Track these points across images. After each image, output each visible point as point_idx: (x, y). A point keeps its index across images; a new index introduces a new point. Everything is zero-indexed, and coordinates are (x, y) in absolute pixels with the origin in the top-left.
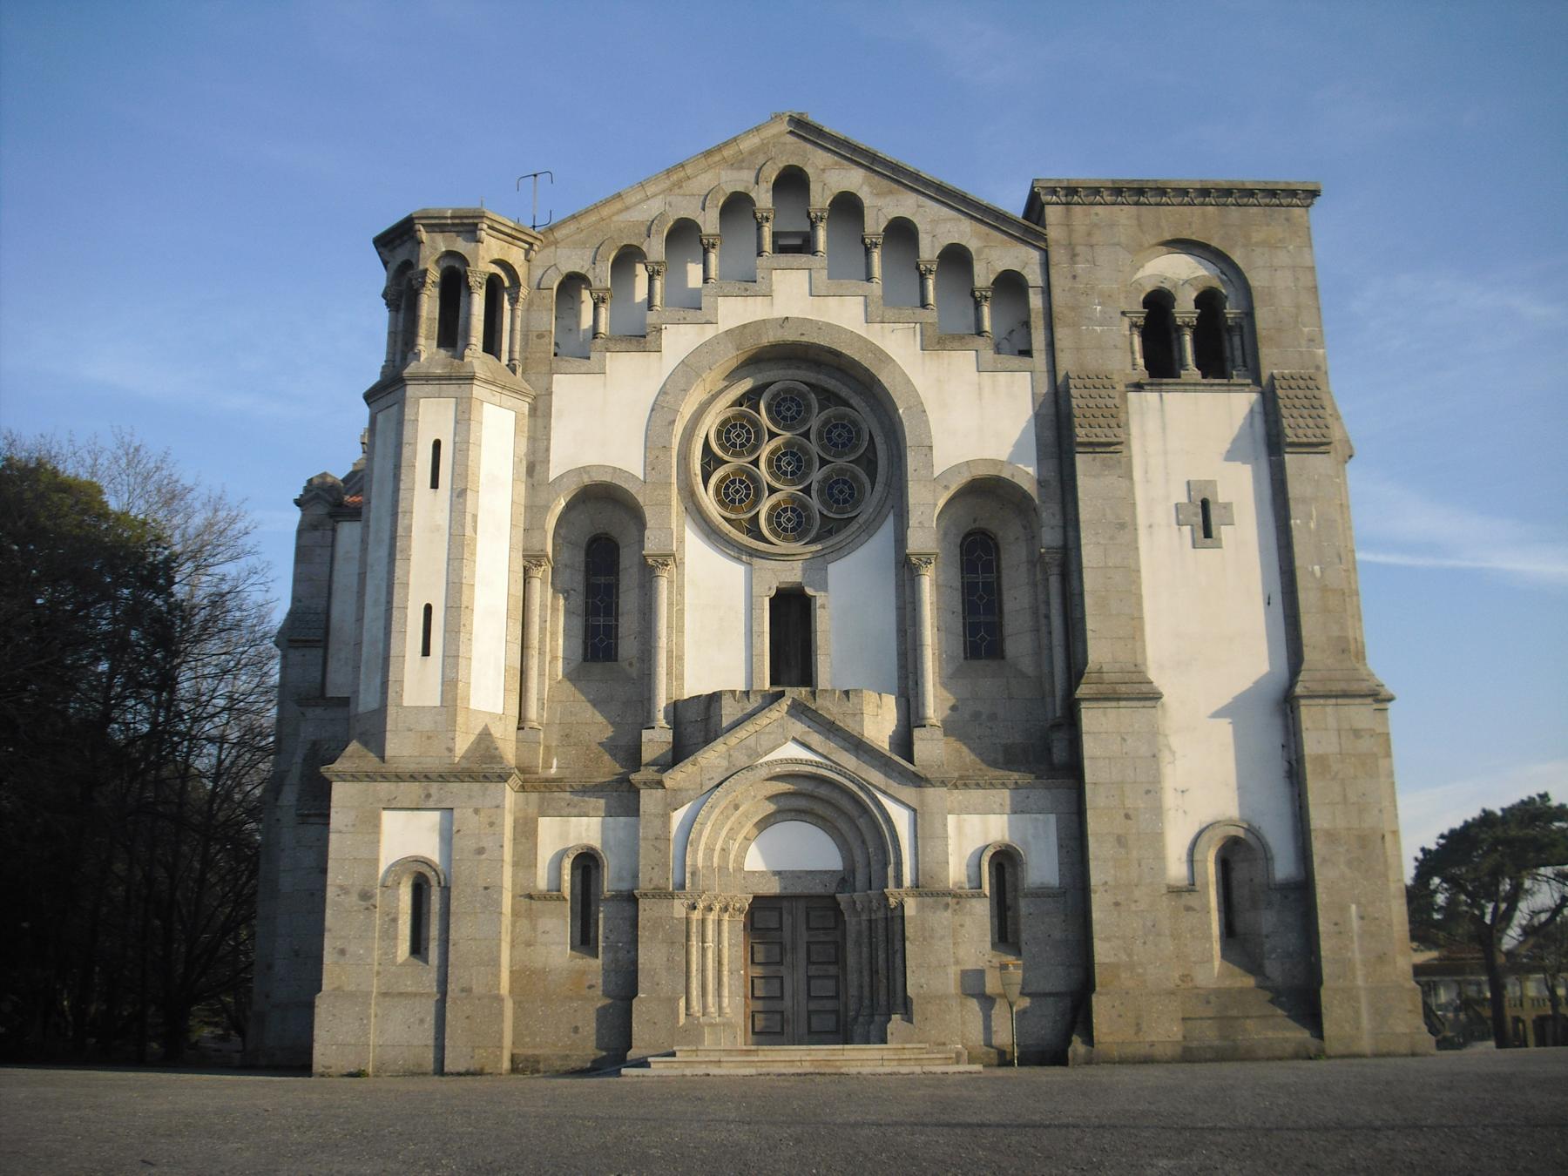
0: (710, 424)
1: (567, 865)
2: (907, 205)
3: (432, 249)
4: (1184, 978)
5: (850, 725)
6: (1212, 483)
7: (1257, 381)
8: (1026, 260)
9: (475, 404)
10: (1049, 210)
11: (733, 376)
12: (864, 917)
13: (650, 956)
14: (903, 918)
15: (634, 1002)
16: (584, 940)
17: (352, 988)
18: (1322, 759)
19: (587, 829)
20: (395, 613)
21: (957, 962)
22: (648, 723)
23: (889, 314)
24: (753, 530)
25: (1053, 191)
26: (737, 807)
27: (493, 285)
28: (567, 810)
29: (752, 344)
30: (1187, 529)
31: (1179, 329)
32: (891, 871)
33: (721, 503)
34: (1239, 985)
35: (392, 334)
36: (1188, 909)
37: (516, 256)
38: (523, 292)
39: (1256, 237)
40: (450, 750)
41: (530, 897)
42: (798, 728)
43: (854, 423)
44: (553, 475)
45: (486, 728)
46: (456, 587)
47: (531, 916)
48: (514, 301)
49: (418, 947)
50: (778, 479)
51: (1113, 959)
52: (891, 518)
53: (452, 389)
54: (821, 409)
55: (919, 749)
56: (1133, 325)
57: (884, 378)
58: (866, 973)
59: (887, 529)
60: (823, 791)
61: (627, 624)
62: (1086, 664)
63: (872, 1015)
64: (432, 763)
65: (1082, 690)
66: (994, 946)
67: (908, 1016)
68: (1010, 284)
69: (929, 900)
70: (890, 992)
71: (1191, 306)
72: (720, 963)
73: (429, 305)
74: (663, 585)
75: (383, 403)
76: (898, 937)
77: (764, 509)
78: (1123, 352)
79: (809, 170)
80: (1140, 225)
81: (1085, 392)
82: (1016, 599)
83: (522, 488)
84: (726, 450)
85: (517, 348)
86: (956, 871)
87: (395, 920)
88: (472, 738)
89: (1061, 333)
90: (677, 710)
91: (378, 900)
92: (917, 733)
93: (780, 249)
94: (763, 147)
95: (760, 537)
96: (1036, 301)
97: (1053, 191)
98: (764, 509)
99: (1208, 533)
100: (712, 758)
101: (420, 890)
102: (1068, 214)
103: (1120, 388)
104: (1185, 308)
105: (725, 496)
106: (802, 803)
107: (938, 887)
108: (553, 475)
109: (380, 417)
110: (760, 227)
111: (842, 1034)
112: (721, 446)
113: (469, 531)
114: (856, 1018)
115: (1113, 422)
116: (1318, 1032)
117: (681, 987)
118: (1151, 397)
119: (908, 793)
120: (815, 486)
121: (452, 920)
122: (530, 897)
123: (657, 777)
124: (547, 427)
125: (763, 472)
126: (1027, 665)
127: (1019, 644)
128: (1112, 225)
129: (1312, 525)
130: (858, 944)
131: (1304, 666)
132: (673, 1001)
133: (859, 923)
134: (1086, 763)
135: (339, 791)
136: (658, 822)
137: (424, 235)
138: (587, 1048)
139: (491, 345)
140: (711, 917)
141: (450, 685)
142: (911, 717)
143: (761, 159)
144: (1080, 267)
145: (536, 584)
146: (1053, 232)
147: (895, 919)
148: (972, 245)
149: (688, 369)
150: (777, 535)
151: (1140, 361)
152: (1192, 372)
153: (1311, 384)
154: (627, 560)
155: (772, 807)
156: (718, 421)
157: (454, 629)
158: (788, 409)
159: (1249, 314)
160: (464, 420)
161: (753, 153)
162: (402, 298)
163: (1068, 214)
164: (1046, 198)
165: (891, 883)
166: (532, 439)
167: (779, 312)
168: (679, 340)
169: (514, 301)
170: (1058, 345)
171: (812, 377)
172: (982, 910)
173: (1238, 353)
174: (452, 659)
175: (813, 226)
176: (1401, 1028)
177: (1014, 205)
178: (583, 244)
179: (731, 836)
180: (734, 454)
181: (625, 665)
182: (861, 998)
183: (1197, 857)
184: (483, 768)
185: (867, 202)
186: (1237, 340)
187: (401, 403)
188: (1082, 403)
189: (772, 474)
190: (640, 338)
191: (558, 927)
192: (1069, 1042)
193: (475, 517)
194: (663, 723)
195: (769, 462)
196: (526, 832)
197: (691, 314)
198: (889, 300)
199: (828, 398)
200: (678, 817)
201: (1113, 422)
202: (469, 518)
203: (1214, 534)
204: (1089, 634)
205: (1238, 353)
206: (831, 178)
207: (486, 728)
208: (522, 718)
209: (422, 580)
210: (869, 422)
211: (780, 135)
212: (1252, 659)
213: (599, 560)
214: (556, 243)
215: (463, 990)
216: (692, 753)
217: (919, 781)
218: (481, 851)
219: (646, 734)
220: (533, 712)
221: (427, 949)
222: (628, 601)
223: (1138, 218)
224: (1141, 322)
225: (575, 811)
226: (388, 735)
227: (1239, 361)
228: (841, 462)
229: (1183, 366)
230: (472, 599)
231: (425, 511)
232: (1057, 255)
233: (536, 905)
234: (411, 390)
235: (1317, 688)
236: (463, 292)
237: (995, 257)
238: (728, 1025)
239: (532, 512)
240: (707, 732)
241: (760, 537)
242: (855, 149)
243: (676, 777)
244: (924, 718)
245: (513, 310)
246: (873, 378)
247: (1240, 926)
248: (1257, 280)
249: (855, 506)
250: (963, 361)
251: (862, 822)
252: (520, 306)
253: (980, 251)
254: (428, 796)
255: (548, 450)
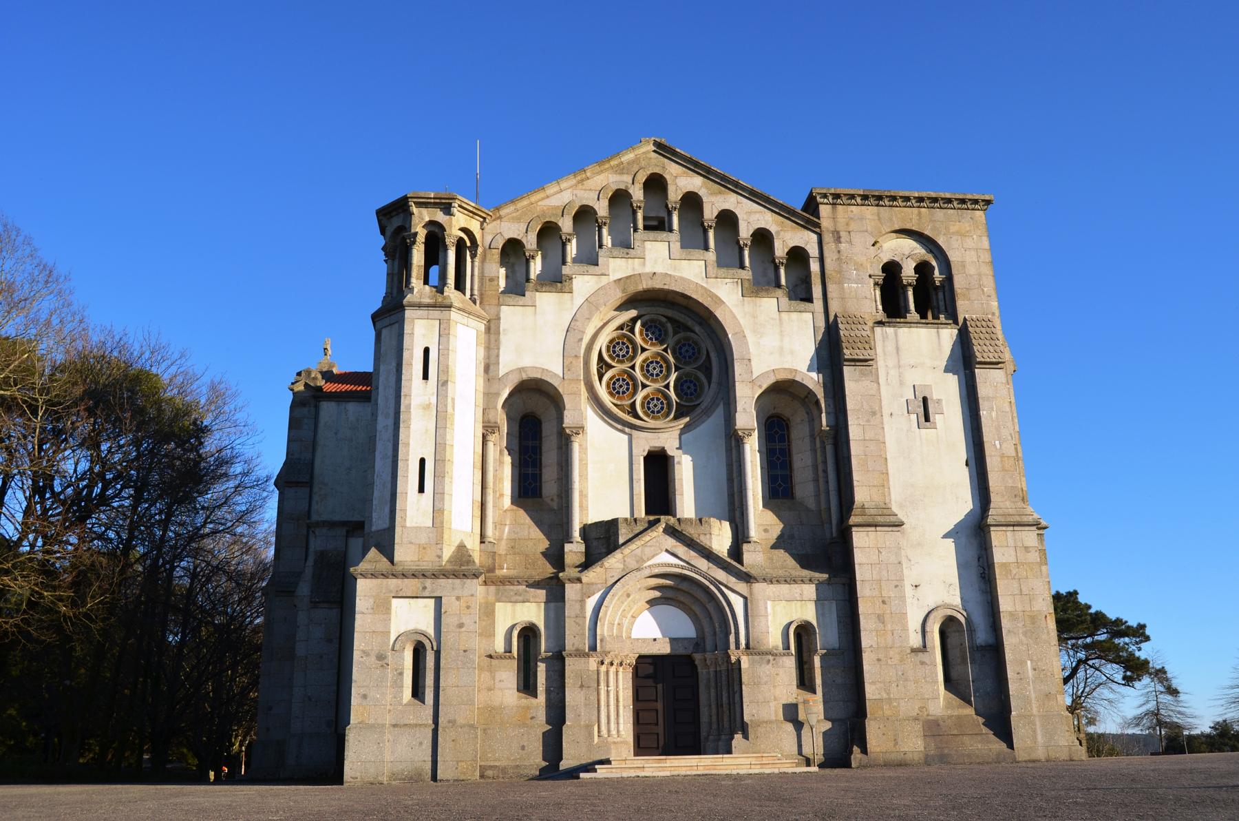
0: (602, 342)
1: (515, 633)
2: (731, 201)
3: (420, 218)
4: (921, 708)
5: (703, 540)
6: (929, 386)
7: (956, 322)
8: (807, 240)
9: (452, 323)
10: (822, 207)
11: (622, 307)
12: (712, 669)
13: (573, 697)
14: (740, 669)
15: (564, 728)
16: (527, 686)
17: (372, 721)
18: (1004, 565)
19: (533, 611)
20: (400, 464)
21: (775, 699)
22: (568, 538)
23: (722, 271)
24: (633, 411)
25: (825, 196)
26: (628, 596)
27: (460, 245)
28: (514, 599)
29: (632, 289)
30: (914, 417)
31: (904, 288)
32: (732, 638)
33: (611, 394)
34: (956, 713)
35: (390, 275)
36: (922, 663)
37: (474, 226)
38: (480, 250)
39: (953, 229)
40: (440, 557)
41: (490, 657)
42: (670, 542)
43: (696, 343)
44: (501, 374)
45: (462, 542)
46: (440, 447)
47: (491, 670)
48: (473, 256)
49: (417, 692)
50: (647, 378)
51: (878, 697)
52: (721, 407)
53: (436, 313)
54: (675, 333)
55: (747, 557)
56: (876, 284)
57: (719, 314)
58: (714, 706)
59: (719, 412)
60: (684, 586)
61: (549, 474)
62: (853, 502)
63: (719, 735)
64: (427, 564)
65: (853, 520)
66: (798, 687)
67: (746, 737)
68: (798, 256)
69: (756, 658)
70: (732, 720)
71: (912, 272)
72: (617, 700)
73: (418, 256)
74: (576, 447)
75: (386, 321)
76: (736, 683)
77: (639, 397)
78: (869, 302)
79: (667, 177)
80: (879, 219)
81: (848, 327)
82: (802, 460)
83: (481, 381)
84: (613, 359)
85: (476, 287)
86: (774, 639)
87: (401, 674)
88: (453, 549)
89: (831, 288)
90: (585, 530)
91: (390, 660)
92: (745, 547)
93: (646, 228)
94: (636, 160)
95: (637, 416)
96: (815, 267)
97: (825, 196)
98: (639, 397)
99: (927, 419)
100: (614, 562)
101: (419, 652)
102: (834, 210)
103: (870, 324)
104: (908, 272)
105: (613, 390)
106: (670, 594)
107: (763, 648)
108: (501, 374)
109: (385, 332)
110: (634, 213)
111: (694, 747)
112: (610, 356)
113: (449, 409)
114: (707, 738)
115: (867, 346)
116: (1011, 745)
117: (595, 718)
118: (890, 331)
119: (741, 587)
120: (672, 384)
121: (442, 673)
122: (490, 657)
123: (578, 575)
124: (498, 341)
125: (638, 373)
126: (811, 503)
127: (804, 487)
128: (862, 219)
129: (994, 414)
130: (708, 687)
131: (992, 505)
132: (589, 727)
133: (708, 673)
134: (857, 567)
135: (362, 585)
136: (578, 606)
137: (414, 209)
138: (536, 760)
139: (460, 286)
140: (612, 669)
141: (438, 512)
142: (740, 537)
143: (635, 168)
144: (843, 246)
145: (490, 445)
146: (826, 222)
147: (735, 671)
148: (773, 229)
149: (591, 304)
150: (648, 416)
151: (880, 307)
152: (913, 315)
153: (990, 324)
154: (548, 430)
155: (657, 594)
156: (608, 340)
157: (439, 476)
158: (655, 330)
159: (949, 279)
160: (444, 333)
161: (630, 163)
162: (398, 252)
163: (834, 210)
164: (819, 199)
165: (732, 646)
166: (488, 348)
167: (648, 269)
168: (584, 284)
169: (473, 256)
170: (829, 295)
171: (670, 313)
172: (790, 663)
173: (942, 303)
174: (439, 495)
175: (670, 214)
176: (1063, 742)
177: (798, 206)
178: (518, 219)
179: (624, 616)
180: (619, 362)
181: (548, 500)
182: (710, 723)
183: (928, 629)
184: (461, 568)
185: (705, 199)
186: (941, 295)
187: (401, 322)
188: (847, 333)
189: (644, 375)
190: (555, 280)
191: (509, 676)
192: (851, 752)
193: (453, 399)
194: (579, 539)
195: (642, 368)
196: (488, 612)
197: (592, 269)
198: (721, 263)
199: (679, 326)
200: (591, 603)
201: (867, 346)
202: (449, 400)
203: (931, 419)
204: (855, 483)
205: (942, 303)
206: (681, 182)
207: (462, 542)
208: (482, 536)
209: (416, 440)
210: (706, 344)
211: (648, 152)
212: (962, 504)
213: (533, 430)
214: (500, 218)
215: (449, 722)
216: (600, 559)
217: (747, 578)
218: (461, 626)
219: (568, 547)
220: (490, 532)
221: (424, 693)
222: (549, 457)
223: (878, 215)
224: (881, 282)
225: (521, 598)
226: (396, 547)
227: (942, 308)
228: (688, 369)
229: (907, 311)
230: (452, 454)
231: (417, 393)
232: (827, 238)
233: (494, 662)
234: (408, 313)
235: (1002, 520)
236: (441, 249)
237: (787, 237)
238: (625, 742)
239: (489, 396)
240: (609, 545)
241: (637, 416)
242: (696, 164)
243: (590, 576)
244: (748, 537)
245: (473, 262)
246: (711, 313)
247: (954, 674)
248: (953, 256)
249: (699, 396)
250: (769, 304)
251: (710, 607)
252: (477, 260)
253: (778, 233)
254: (425, 588)
255: (498, 356)
